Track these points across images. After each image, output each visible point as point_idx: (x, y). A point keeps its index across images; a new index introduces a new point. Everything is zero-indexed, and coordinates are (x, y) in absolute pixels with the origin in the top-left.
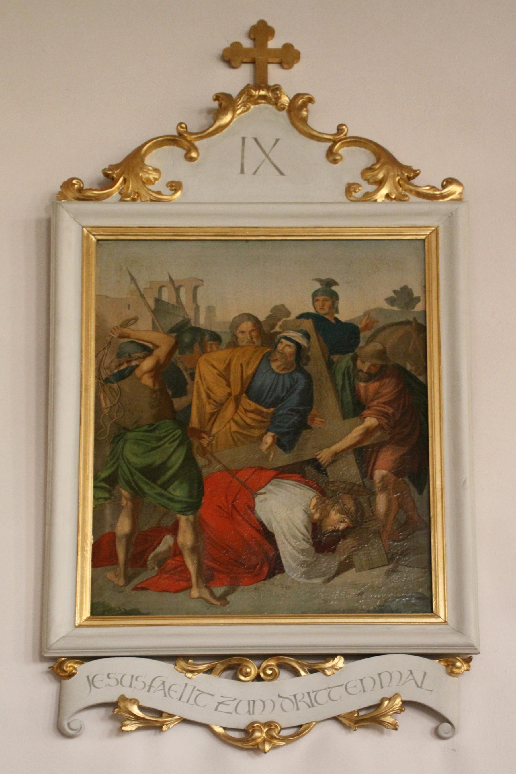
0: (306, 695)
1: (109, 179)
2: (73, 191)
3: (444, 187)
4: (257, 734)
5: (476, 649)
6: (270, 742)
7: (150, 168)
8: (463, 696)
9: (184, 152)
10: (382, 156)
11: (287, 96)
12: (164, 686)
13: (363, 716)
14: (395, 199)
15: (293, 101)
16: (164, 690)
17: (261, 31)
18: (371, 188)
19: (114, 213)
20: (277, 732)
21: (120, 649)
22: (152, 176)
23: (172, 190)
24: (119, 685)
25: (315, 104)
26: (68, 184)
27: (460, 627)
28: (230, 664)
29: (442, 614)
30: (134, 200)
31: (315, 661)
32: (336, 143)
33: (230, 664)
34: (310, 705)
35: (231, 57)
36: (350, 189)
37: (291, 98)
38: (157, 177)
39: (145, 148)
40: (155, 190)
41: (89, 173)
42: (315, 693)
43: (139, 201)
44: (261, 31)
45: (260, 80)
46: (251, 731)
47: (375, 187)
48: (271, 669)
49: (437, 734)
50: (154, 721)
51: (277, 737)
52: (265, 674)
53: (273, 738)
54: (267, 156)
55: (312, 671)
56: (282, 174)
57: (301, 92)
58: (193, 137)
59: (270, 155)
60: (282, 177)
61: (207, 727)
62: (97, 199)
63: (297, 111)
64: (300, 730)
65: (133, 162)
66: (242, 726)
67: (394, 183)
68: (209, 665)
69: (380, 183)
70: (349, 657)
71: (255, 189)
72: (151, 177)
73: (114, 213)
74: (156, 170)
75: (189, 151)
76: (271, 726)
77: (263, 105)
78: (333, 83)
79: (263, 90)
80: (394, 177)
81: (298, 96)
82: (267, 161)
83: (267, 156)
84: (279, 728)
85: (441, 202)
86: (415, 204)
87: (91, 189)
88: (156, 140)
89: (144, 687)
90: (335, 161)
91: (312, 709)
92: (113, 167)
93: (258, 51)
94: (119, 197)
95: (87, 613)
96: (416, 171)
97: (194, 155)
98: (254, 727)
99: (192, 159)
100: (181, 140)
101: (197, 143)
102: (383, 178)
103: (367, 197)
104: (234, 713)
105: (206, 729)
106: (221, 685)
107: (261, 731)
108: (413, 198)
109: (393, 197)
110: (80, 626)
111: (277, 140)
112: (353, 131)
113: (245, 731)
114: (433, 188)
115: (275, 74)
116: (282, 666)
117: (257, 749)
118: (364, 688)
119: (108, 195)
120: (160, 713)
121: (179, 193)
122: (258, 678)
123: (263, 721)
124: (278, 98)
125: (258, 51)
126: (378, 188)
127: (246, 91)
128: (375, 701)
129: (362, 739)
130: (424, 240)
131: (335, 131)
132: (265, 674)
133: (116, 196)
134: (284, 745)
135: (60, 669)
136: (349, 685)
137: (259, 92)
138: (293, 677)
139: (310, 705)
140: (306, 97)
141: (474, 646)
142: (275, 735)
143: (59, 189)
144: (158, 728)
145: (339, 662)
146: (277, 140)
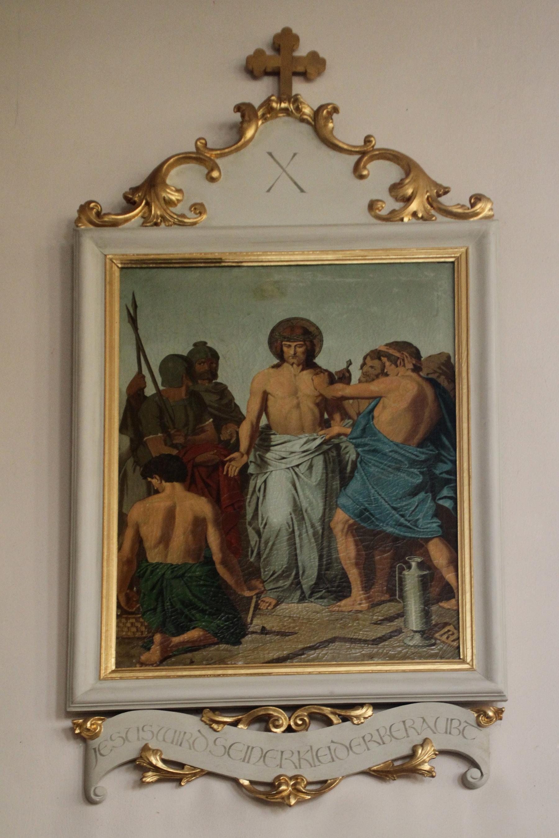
0: (296, 755)
1: (130, 203)
2: (91, 215)
3: (473, 205)
4: (283, 787)
5: (505, 696)
6: (296, 796)
7: (173, 188)
8: (498, 746)
9: (206, 171)
10: (408, 166)
11: (309, 106)
12: (426, 723)
13: (397, 766)
14: (422, 218)
15: (317, 113)
16: (429, 727)
17: (285, 41)
18: (398, 205)
19: (139, 239)
20: (303, 786)
21: (163, 701)
22: (174, 196)
23: (196, 214)
24: (351, 752)
25: (340, 115)
26: (84, 208)
27: (488, 673)
28: (257, 716)
29: (469, 659)
30: (156, 224)
31: (345, 709)
32: (366, 154)
33: (257, 716)
34: (297, 765)
35: (253, 69)
36: (372, 206)
37: (315, 109)
38: (179, 198)
39: (165, 167)
40: (179, 213)
41: (108, 197)
42: (466, 724)
43: (163, 225)
44: (285, 41)
45: (285, 93)
46: (277, 784)
47: (401, 204)
48: (301, 720)
49: (465, 783)
50: (175, 774)
51: (304, 791)
52: (296, 724)
53: (299, 791)
54: (284, 171)
55: (345, 719)
56: (302, 191)
57: (323, 102)
58: (214, 153)
59: (287, 170)
60: (303, 194)
61: (235, 781)
62: (114, 224)
63: (319, 123)
64: (324, 786)
65: (154, 182)
66: (269, 779)
67: (422, 201)
68: (234, 718)
69: (408, 200)
70: (378, 707)
71: (283, 212)
72: (173, 198)
73: (139, 239)
74: (179, 191)
75: (212, 170)
76: (297, 779)
77: (283, 118)
78: (360, 94)
79: (285, 103)
80: (422, 195)
81: (321, 108)
82: (284, 174)
83: (284, 171)
84: (305, 782)
85: (473, 221)
86: (443, 225)
87: (109, 214)
88: (176, 158)
89: (153, 736)
90: (361, 177)
91: (313, 768)
92: (135, 190)
93: (282, 64)
94: (142, 220)
95: (112, 665)
96: (446, 188)
97: (215, 174)
98: (280, 780)
99: (212, 180)
100: (201, 157)
101: (219, 161)
102: (413, 193)
103: (392, 217)
104: (462, 721)
105: (234, 784)
106: (246, 734)
107: (287, 785)
108: (440, 218)
109: (420, 215)
110: (105, 679)
111: (295, 155)
112: (380, 143)
113: (271, 785)
114: (463, 206)
115: (299, 87)
116: (312, 716)
117: (283, 804)
118: (281, 764)
119: (127, 220)
120: (181, 766)
121: (204, 217)
122: (289, 730)
123: (291, 774)
124: (298, 109)
125: (282, 64)
126: (405, 206)
127: (267, 103)
128: (406, 751)
129: (399, 787)
130: (453, 263)
131: (362, 143)
132: (296, 724)
133: (138, 220)
134: (309, 800)
135: (82, 721)
136: (374, 737)
137: (280, 104)
138: (323, 727)
139: (297, 765)
140: (329, 107)
141: (503, 693)
142: (302, 789)
143: (76, 215)
144: (177, 780)
145: (368, 712)
146: (269, 191)
